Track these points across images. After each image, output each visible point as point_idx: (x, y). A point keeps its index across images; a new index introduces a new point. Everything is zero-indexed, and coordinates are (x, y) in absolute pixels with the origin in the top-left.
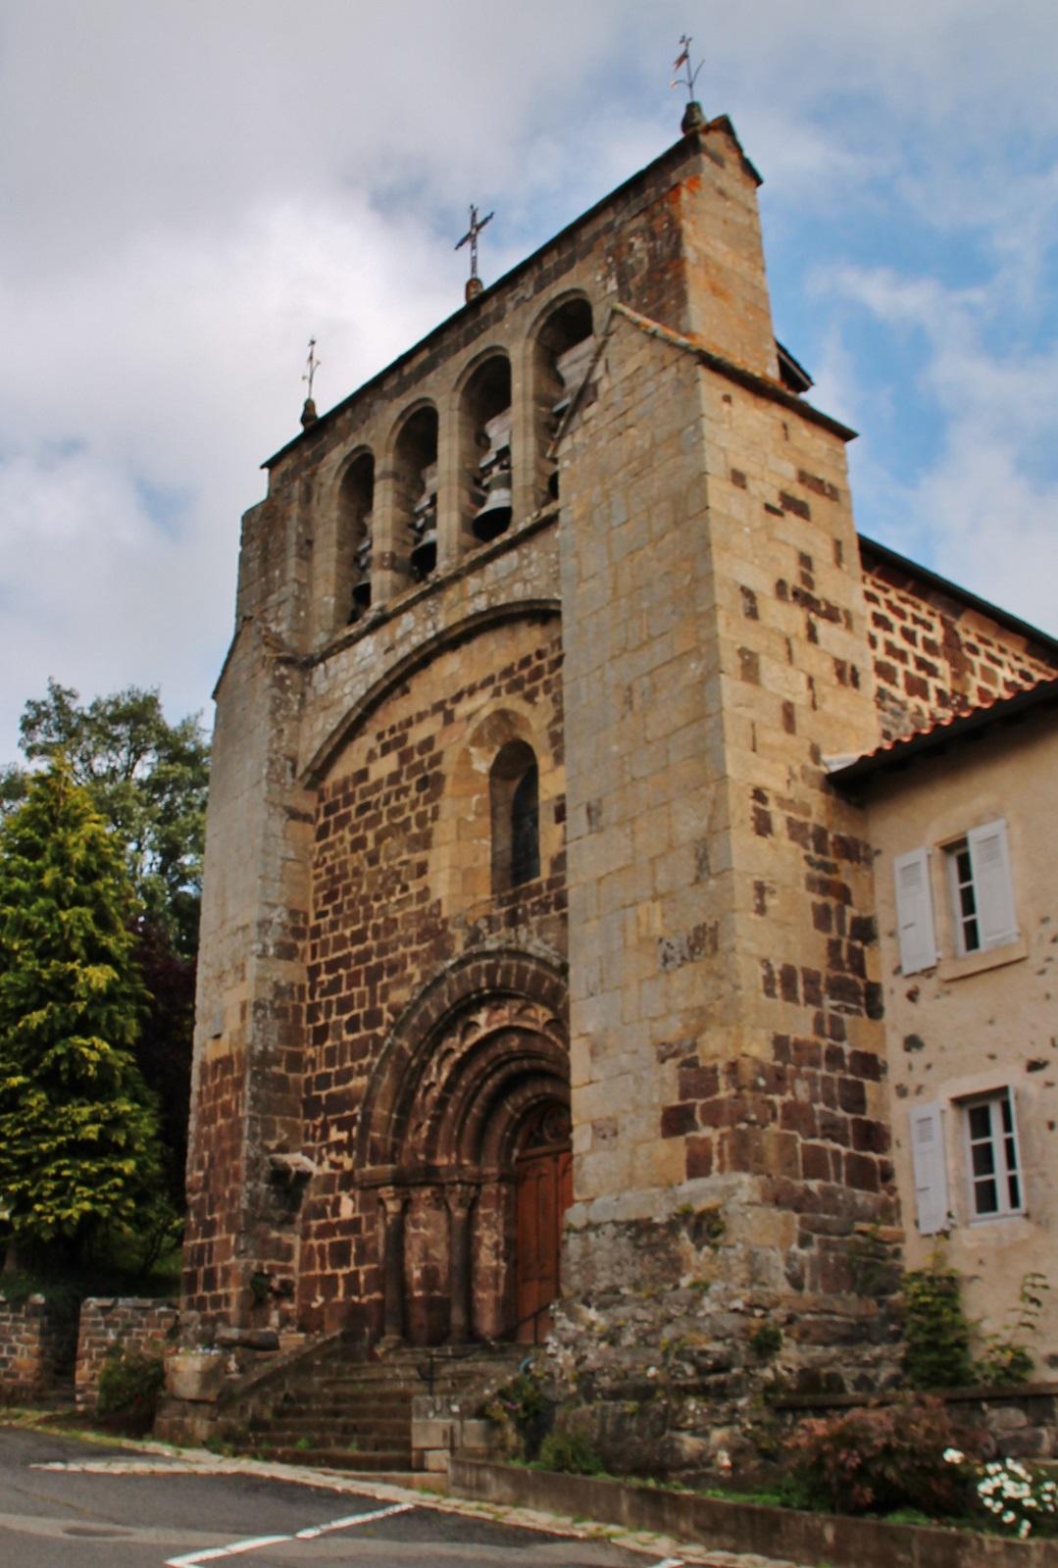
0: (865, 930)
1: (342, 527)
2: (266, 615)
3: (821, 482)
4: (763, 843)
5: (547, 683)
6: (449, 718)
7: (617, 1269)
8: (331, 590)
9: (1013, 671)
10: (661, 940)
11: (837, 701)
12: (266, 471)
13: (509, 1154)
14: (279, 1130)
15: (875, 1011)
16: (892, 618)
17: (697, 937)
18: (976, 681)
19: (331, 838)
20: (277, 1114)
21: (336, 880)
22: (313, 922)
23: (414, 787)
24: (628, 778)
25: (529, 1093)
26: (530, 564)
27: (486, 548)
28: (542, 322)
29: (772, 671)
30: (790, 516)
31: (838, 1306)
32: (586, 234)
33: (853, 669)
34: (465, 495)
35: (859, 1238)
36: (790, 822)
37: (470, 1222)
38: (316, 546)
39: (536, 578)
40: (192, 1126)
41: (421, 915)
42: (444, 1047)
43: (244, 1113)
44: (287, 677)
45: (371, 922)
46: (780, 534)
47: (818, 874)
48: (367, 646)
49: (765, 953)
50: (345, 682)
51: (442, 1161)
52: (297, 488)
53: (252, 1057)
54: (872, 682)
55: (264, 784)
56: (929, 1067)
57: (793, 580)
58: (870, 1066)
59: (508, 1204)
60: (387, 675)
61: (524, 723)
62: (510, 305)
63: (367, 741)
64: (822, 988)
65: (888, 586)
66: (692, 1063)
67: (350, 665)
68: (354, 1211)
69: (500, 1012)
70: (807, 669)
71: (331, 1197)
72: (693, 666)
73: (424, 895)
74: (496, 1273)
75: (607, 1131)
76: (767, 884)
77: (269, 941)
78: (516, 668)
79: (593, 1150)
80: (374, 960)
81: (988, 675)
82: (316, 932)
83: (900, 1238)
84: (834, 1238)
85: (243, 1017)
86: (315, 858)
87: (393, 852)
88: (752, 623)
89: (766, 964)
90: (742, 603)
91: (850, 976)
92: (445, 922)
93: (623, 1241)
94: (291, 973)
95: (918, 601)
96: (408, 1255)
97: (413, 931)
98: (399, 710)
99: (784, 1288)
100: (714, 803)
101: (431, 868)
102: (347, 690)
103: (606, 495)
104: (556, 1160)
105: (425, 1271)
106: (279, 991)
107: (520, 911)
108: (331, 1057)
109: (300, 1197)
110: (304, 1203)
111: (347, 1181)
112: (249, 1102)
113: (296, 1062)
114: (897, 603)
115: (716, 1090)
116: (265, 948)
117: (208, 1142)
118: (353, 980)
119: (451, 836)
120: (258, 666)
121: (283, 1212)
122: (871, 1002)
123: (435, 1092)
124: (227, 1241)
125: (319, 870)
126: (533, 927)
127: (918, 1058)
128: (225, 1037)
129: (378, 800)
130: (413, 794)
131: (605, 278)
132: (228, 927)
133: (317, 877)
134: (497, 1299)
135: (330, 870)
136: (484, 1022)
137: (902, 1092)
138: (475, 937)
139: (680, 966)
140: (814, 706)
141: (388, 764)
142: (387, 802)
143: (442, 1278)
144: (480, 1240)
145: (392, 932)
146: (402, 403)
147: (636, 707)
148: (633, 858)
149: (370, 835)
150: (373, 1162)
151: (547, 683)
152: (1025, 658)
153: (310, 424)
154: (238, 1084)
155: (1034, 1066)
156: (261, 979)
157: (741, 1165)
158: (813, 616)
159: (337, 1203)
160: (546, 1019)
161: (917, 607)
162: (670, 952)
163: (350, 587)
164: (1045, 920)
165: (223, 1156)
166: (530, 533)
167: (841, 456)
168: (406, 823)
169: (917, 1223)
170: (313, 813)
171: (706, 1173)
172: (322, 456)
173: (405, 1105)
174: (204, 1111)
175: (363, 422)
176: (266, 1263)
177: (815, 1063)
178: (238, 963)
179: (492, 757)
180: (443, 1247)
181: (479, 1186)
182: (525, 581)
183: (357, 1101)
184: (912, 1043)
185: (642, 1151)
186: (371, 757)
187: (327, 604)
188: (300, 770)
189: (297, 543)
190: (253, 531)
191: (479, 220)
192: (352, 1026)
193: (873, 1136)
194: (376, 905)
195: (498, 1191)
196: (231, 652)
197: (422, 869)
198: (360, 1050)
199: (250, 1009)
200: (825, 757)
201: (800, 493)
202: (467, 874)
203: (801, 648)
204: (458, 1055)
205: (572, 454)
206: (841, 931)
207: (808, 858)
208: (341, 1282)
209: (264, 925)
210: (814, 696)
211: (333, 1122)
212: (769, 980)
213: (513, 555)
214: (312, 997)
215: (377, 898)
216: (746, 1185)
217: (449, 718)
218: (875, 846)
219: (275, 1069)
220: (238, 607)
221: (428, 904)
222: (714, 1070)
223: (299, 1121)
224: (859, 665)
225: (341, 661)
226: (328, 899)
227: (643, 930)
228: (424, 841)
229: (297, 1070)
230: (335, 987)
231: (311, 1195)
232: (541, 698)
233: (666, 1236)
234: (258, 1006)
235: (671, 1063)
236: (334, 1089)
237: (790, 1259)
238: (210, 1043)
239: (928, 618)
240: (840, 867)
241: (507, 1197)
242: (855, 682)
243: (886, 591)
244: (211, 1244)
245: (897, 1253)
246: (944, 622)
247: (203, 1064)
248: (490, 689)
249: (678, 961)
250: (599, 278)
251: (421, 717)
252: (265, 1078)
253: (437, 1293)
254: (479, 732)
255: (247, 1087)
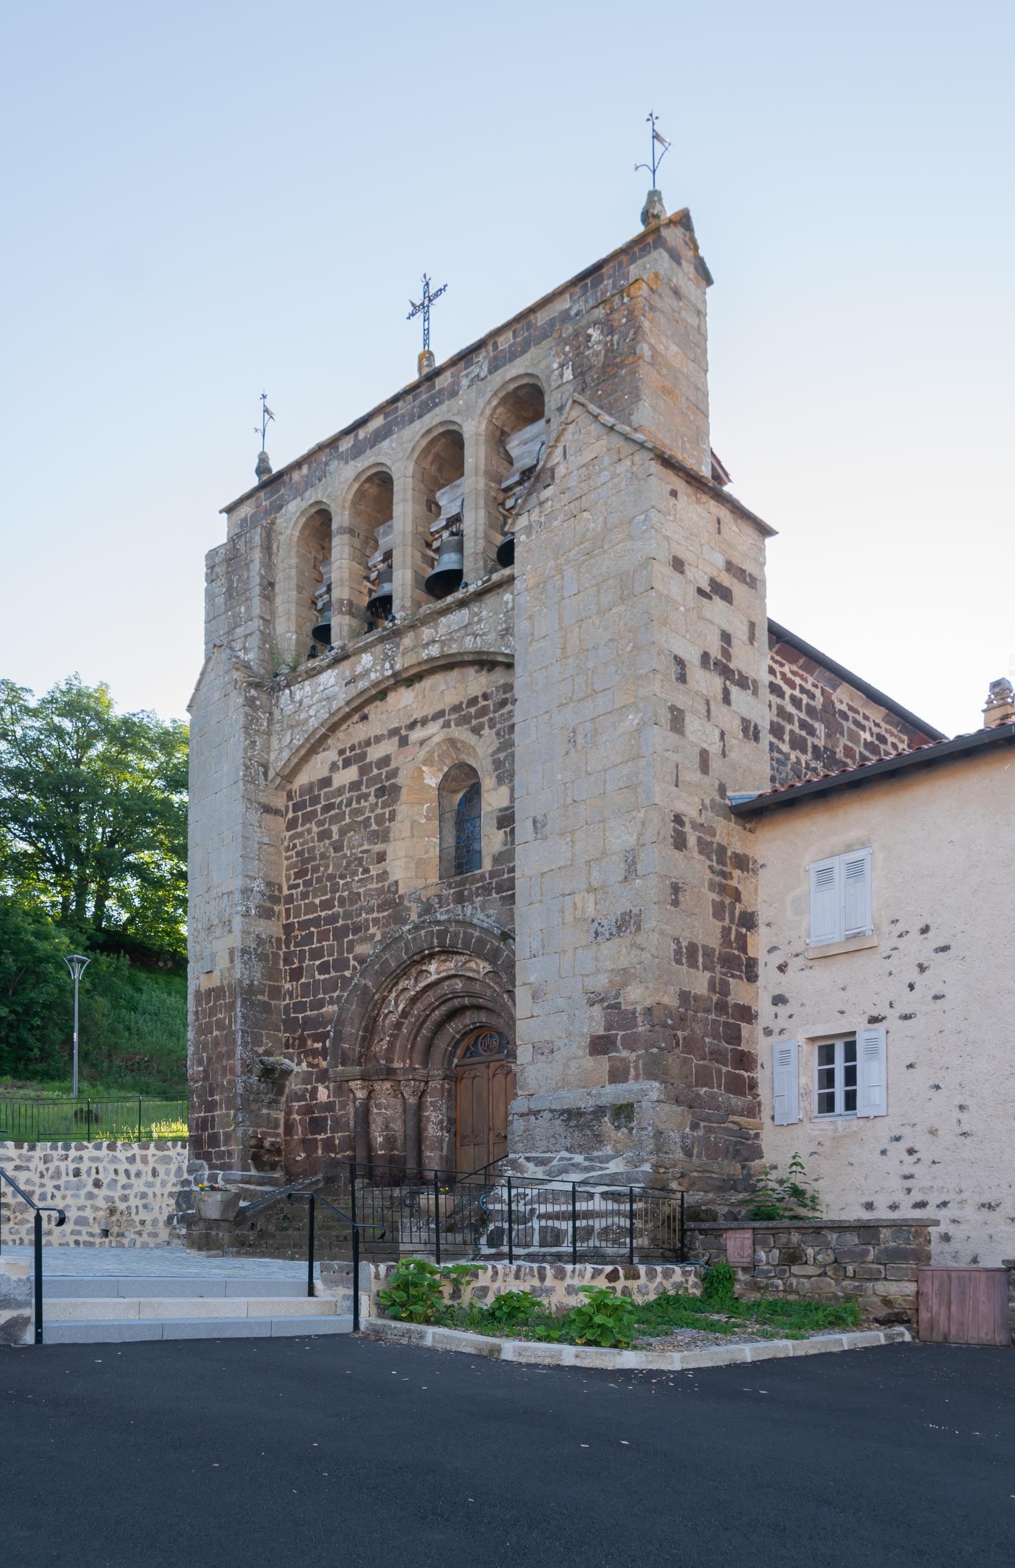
0: (749, 921)
1: (300, 573)
2: (234, 644)
3: (743, 571)
4: (678, 855)
5: (491, 720)
6: (404, 742)
7: (552, 1140)
8: (293, 628)
9: (872, 735)
10: (593, 921)
11: (741, 751)
12: (225, 515)
13: (450, 1062)
14: (265, 1040)
15: (752, 977)
16: (785, 687)
17: (623, 920)
18: (844, 741)
19: (300, 829)
20: (264, 1029)
21: (304, 861)
22: (286, 892)
23: (373, 793)
24: (569, 800)
25: (468, 1019)
26: (480, 621)
27: (440, 604)
28: (494, 403)
29: (693, 724)
30: (716, 598)
31: (716, 1167)
32: (542, 318)
33: (756, 727)
34: (418, 555)
35: (731, 1125)
36: (699, 840)
37: (420, 1107)
38: (277, 588)
39: (484, 634)
40: (190, 1035)
41: (380, 891)
42: (400, 987)
43: (237, 1026)
44: (257, 699)
45: (337, 895)
46: (707, 614)
47: (718, 879)
48: (329, 678)
49: (677, 934)
50: (310, 707)
51: (397, 1065)
52: (257, 537)
53: (242, 988)
54: (766, 738)
55: (241, 783)
56: (791, 1016)
57: (715, 653)
58: (747, 1014)
59: (449, 1095)
60: (348, 703)
61: (472, 750)
62: (465, 382)
63: (330, 755)
64: (716, 960)
65: (784, 662)
66: (617, 1006)
67: (314, 693)
68: (329, 1097)
69: (448, 964)
70: (721, 725)
71: (309, 1087)
72: (631, 717)
73: (383, 876)
74: (441, 1140)
75: (544, 1050)
76: (680, 885)
77: (251, 905)
78: (464, 706)
79: (533, 1062)
80: (341, 922)
81: (854, 737)
82: (290, 899)
83: (761, 1126)
84: (715, 1125)
85: (232, 961)
86: (286, 844)
87: (356, 843)
88: (681, 686)
89: (677, 940)
90: (673, 670)
91: (736, 952)
92: (401, 897)
93: (558, 1122)
94: (272, 928)
95: (805, 675)
96: (373, 1127)
97: (374, 902)
98: (358, 732)
99: (679, 1155)
100: (643, 823)
101: (389, 857)
102: (312, 712)
103: (559, 569)
104: (488, 1067)
105: (387, 1139)
106: (260, 941)
107: (466, 893)
108: (305, 989)
109: (283, 1086)
110: (287, 1090)
111: (323, 1076)
112: (239, 1020)
113: (276, 993)
114: (789, 675)
115: (636, 1026)
116: (248, 909)
117: (205, 1047)
118: (323, 936)
119: (407, 833)
120: (230, 687)
121: (271, 1096)
122: (750, 971)
123: (393, 1018)
124: (228, 1115)
125: (289, 853)
126: (477, 905)
127: (783, 1010)
128: (217, 973)
129: (341, 802)
130: (372, 799)
131: (562, 366)
132: (214, 892)
133: (287, 858)
134: (441, 1157)
135: (299, 854)
136: (434, 969)
137: (768, 1032)
138: (427, 909)
139: (608, 940)
140: (724, 755)
141: (350, 774)
142: (349, 804)
143: (399, 1143)
144: (428, 1118)
145: (356, 903)
146: (360, 464)
147: (579, 746)
148: (572, 860)
149: (335, 829)
150: (343, 1064)
151: (491, 720)
152: (883, 724)
153: (265, 477)
154: (231, 1007)
155: (874, 1020)
156: (246, 933)
157: (650, 1076)
158: (728, 683)
159: (315, 1091)
160: (486, 971)
161: (806, 680)
162: (600, 929)
163: (309, 627)
164: (895, 922)
165: (220, 1056)
166: (480, 595)
167: (762, 550)
168: (366, 822)
169: (773, 1118)
170: (283, 809)
171: (625, 1080)
172: (281, 507)
173: (371, 1029)
174: (201, 1025)
175: (320, 480)
176: (259, 1130)
177: (708, 1011)
178: (226, 918)
179: (441, 776)
180: (399, 1122)
181: (427, 1082)
182: (475, 636)
183: (330, 1022)
184: (779, 1000)
185: (573, 1065)
186: (334, 767)
187: (290, 639)
188: (271, 774)
189: (261, 585)
190: (217, 569)
191: (432, 291)
192: (324, 968)
193: (745, 1060)
194: (341, 882)
195: (442, 1086)
196: (203, 674)
197: (381, 857)
198: (330, 986)
199: (237, 954)
200: (729, 794)
201: (726, 580)
202: (420, 864)
203: (718, 709)
204: (413, 993)
205: (528, 529)
206: (732, 921)
207: (710, 867)
208: (320, 1144)
209: (246, 892)
210: (724, 745)
211: (309, 1036)
212: (678, 952)
213: (465, 612)
214: (288, 947)
215: (342, 877)
216: (654, 1089)
217: (404, 742)
218: (761, 862)
219: (260, 997)
220: (206, 635)
221: (386, 884)
222: (634, 1012)
223: (281, 1035)
224: (760, 722)
225: (303, 691)
226: (298, 876)
227: (578, 913)
228: (383, 836)
229: (278, 999)
230: (308, 939)
231: (293, 1085)
232: (486, 731)
233: (592, 1120)
234: (244, 951)
235: (597, 1007)
236: (308, 1013)
237: (684, 1137)
238: (202, 977)
239: (813, 689)
240: (734, 875)
241: (449, 1090)
242: (756, 738)
243: (782, 665)
244: (213, 1117)
245: (757, 1136)
246: (823, 692)
247: (198, 992)
248: (441, 721)
249: (608, 936)
250: (555, 366)
251: (378, 739)
252: (252, 1003)
253: (396, 1152)
254: (431, 753)
255: (238, 1009)
